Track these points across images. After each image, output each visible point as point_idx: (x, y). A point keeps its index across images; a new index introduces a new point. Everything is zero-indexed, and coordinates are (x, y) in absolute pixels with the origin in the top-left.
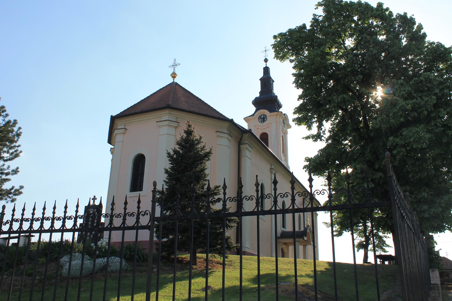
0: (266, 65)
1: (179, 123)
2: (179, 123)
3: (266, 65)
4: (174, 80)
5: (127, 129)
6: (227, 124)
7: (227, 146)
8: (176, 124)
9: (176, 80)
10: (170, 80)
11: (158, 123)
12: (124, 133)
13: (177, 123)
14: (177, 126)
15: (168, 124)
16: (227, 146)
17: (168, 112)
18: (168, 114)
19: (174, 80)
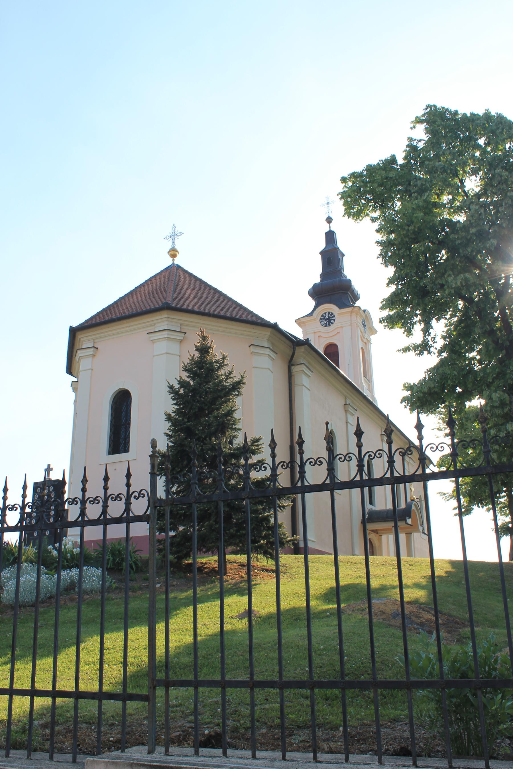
0: (330, 227)
1: (185, 333)
2: (185, 333)
3: (330, 227)
4: (173, 260)
5: (97, 348)
6: (268, 332)
7: (269, 369)
8: (180, 336)
9: (178, 261)
10: (168, 262)
11: (151, 335)
12: (94, 356)
13: (183, 335)
14: (182, 338)
15: (166, 336)
16: (269, 369)
17: (166, 316)
18: (166, 319)
19: (173, 260)
